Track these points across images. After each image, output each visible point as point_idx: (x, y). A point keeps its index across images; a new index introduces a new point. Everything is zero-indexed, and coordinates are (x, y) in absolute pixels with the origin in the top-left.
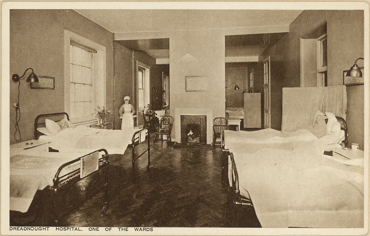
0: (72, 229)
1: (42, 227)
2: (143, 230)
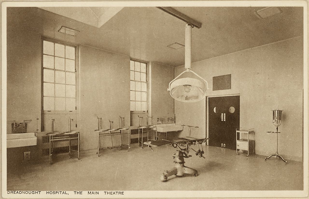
1: (35, 191)
2: (94, 193)
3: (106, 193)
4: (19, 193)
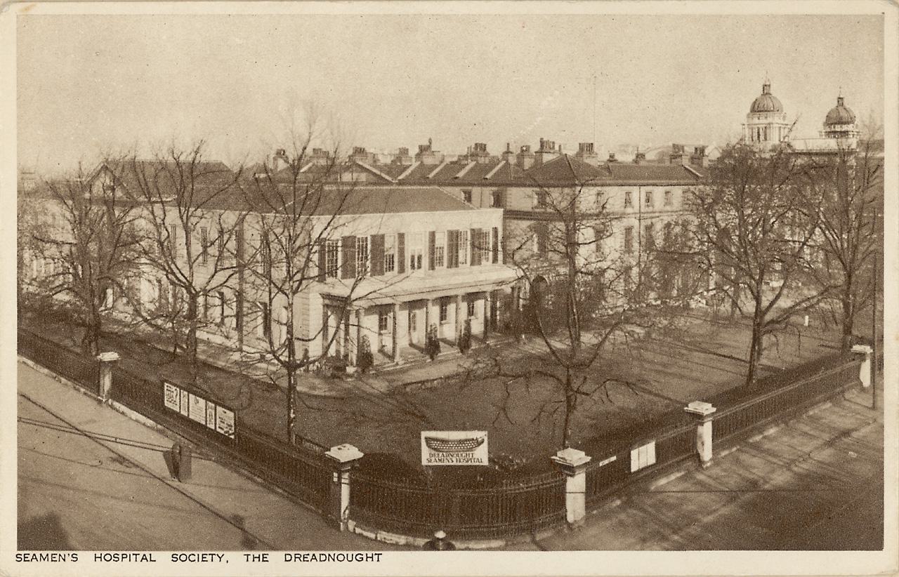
0: (133, 558)
2: (39, 559)
3: (251, 558)
4: (318, 560)
